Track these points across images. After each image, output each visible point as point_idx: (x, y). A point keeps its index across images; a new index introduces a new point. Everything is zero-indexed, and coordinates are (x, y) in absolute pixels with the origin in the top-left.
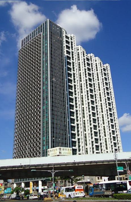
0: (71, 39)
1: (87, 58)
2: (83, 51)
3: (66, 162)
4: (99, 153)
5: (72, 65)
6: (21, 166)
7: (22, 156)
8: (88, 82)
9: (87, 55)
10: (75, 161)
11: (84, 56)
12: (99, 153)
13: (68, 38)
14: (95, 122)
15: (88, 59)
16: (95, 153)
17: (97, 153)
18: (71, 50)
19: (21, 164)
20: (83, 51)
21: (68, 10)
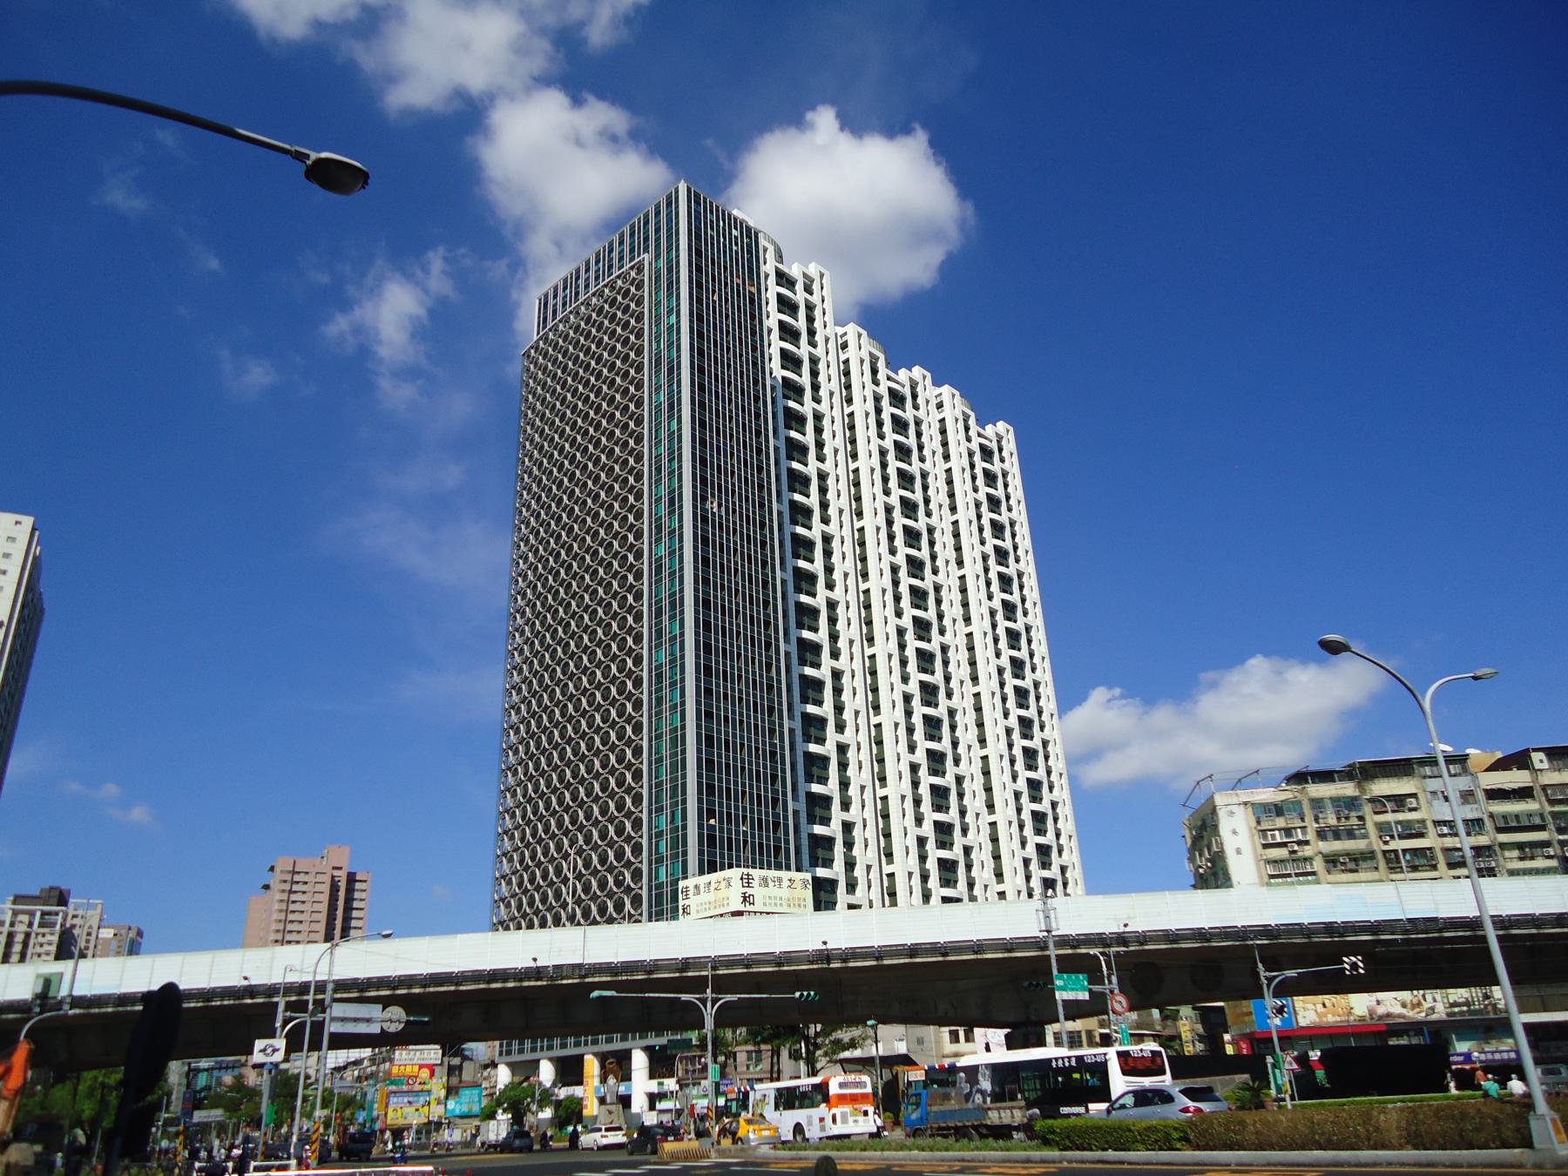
4: (958, 900)
12: (958, 900)
17: (946, 900)
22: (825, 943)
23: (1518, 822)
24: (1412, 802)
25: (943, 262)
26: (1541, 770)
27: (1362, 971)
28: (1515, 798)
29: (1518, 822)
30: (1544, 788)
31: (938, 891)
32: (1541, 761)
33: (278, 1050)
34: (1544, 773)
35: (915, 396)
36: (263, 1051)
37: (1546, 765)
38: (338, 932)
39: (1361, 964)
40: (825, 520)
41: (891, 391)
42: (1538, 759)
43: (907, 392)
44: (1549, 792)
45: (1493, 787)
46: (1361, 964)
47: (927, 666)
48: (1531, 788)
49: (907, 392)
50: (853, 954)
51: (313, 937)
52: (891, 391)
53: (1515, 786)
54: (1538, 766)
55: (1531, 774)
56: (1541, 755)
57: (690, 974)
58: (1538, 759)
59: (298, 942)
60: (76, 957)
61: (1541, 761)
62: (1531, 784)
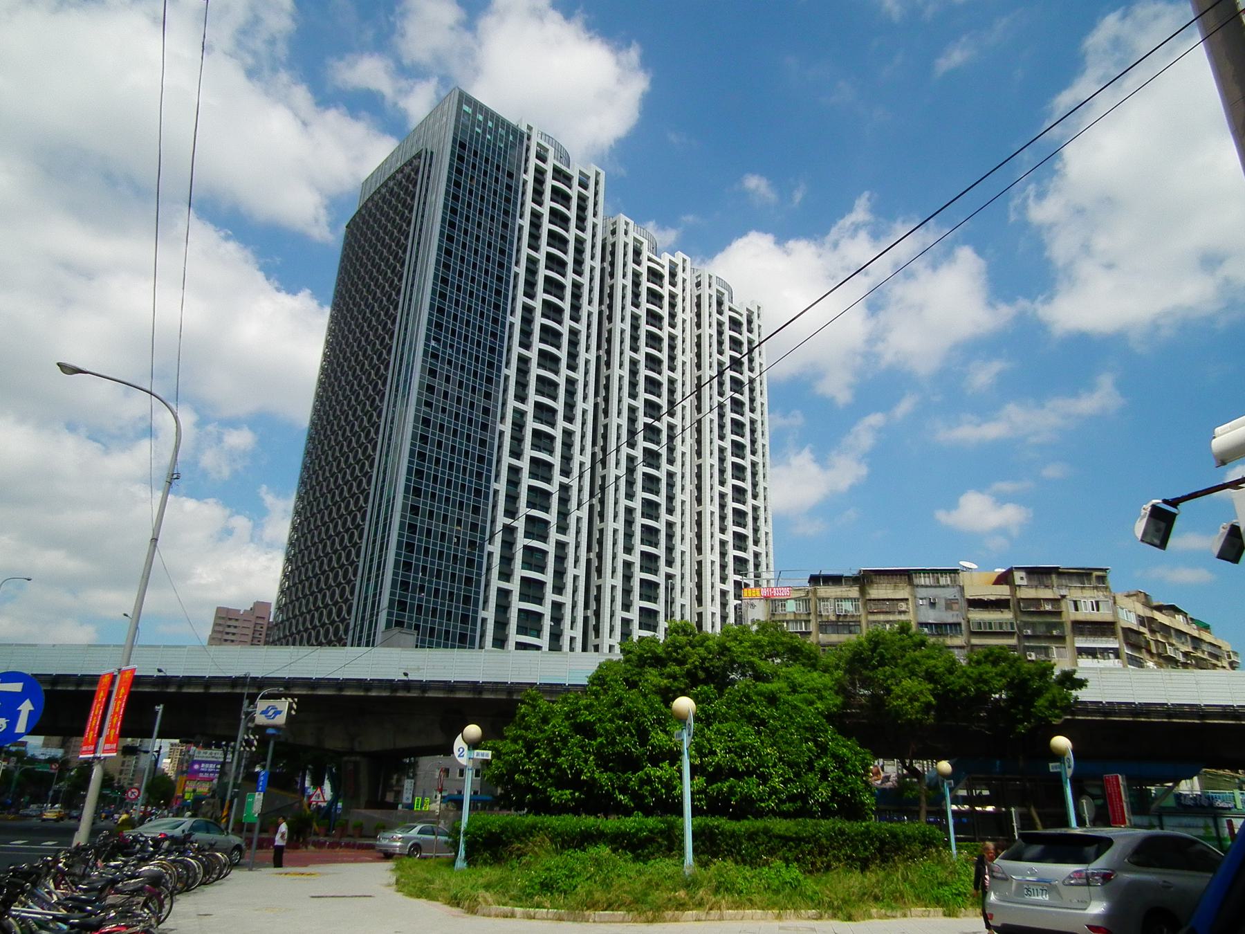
0: (584, 185)
1: (731, 318)
2: (718, 291)
3: (207, 673)
4: (538, 648)
5: (746, 389)
6: (407, 685)
7: (288, 641)
8: (729, 415)
9: (654, 257)
10: (411, 677)
11: (720, 312)
12: (538, 648)
13: (567, 179)
14: (653, 539)
15: (655, 275)
16: (511, 644)
17: (521, 646)
18: (665, 291)
19: (406, 674)
20: (718, 291)
21: (562, 17)
22: (406, 674)
23: (1001, 628)
24: (903, 606)
25: (757, 231)
26: (1019, 586)
27: (254, 749)
28: (992, 608)
29: (991, 628)
30: (1020, 600)
31: (513, 637)
32: (1022, 578)
33: (263, 713)
34: (1022, 588)
35: (750, 322)
36: (278, 713)
37: (1025, 582)
38: (364, 640)
39: (255, 743)
40: (752, 410)
41: (732, 319)
42: (1019, 578)
43: (744, 320)
44: (1022, 604)
45: (976, 598)
46: (255, 743)
47: (740, 497)
48: (1008, 600)
49: (744, 320)
50: (189, 680)
51: (243, 639)
52: (732, 319)
53: (993, 598)
54: (1018, 582)
55: (1011, 589)
56: (1023, 574)
57: (59, 688)
58: (1019, 578)
59: (232, 641)
60: (1076, 668)
61: (1022, 578)
62: (1009, 597)
